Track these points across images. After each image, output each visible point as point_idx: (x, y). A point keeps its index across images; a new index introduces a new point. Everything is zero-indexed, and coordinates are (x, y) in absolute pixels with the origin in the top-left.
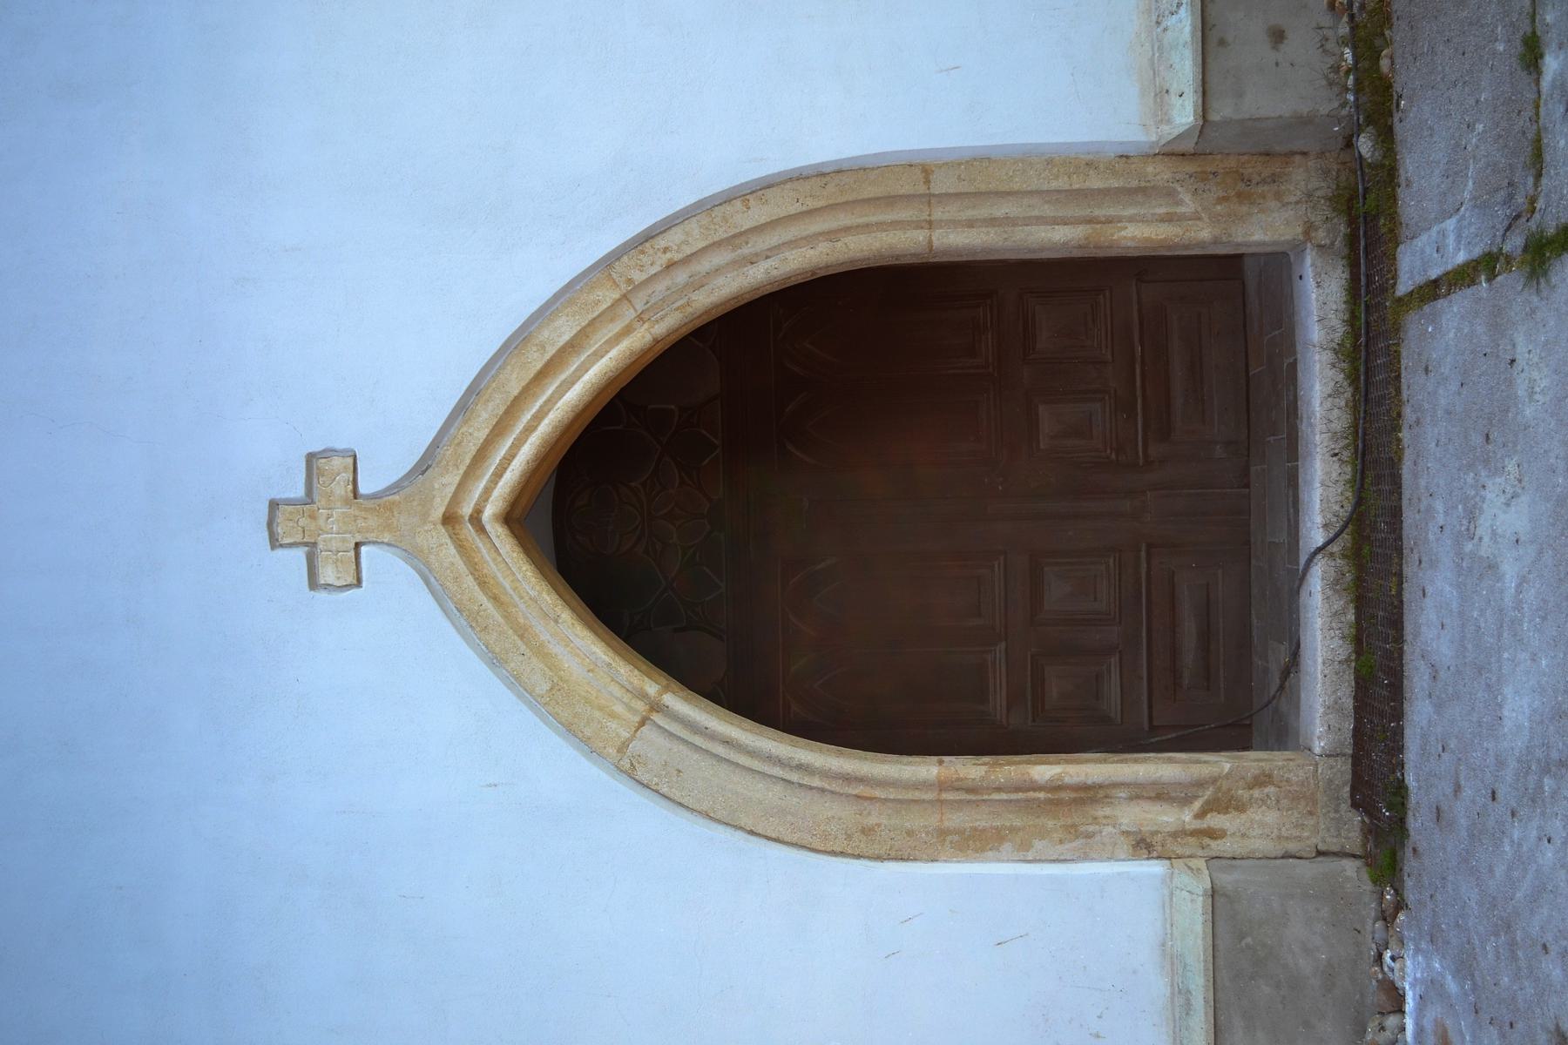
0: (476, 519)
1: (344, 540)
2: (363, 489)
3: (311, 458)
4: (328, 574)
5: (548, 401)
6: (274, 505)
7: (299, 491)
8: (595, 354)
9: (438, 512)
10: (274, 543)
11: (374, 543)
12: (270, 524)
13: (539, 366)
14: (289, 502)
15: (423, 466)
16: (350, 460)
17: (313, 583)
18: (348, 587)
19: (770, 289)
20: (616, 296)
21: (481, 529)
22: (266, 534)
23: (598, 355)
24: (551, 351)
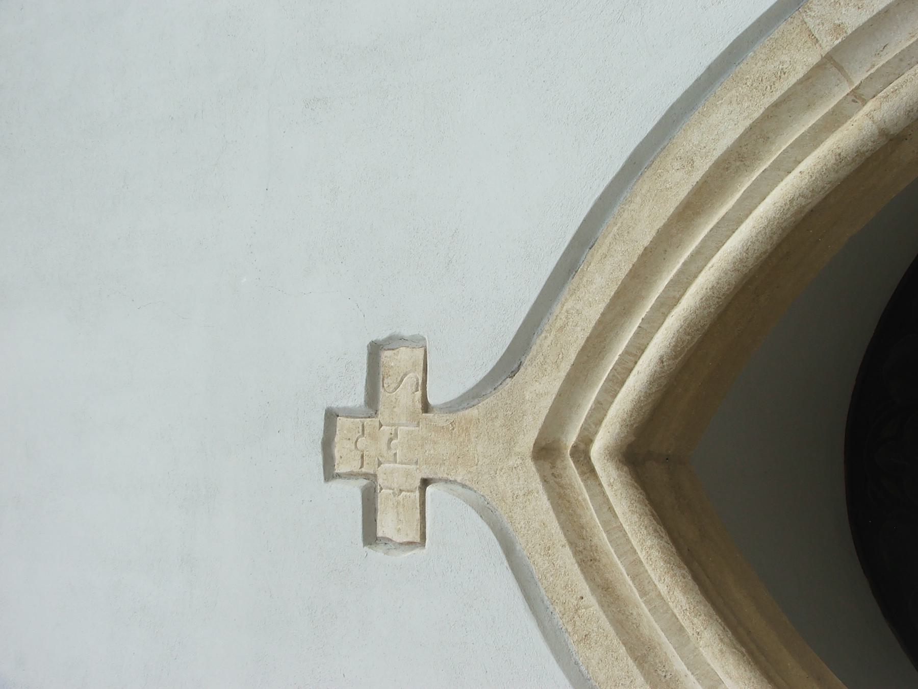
0: (581, 454)
1: (408, 474)
2: (431, 401)
3: (375, 350)
4: (386, 526)
5: (698, 252)
6: (331, 417)
7: (357, 398)
8: (776, 165)
9: (527, 440)
10: (330, 473)
11: (446, 481)
12: (327, 445)
13: (683, 192)
14: (350, 413)
15: (511, 363)
16: (420, 353)
17: (370, 536)
18: (411, 544)
19: (843, 173)
20: (813, 58)
21: (588, 471)
22: (320, 459)
23: (782, 168)
24: (703, 166)
